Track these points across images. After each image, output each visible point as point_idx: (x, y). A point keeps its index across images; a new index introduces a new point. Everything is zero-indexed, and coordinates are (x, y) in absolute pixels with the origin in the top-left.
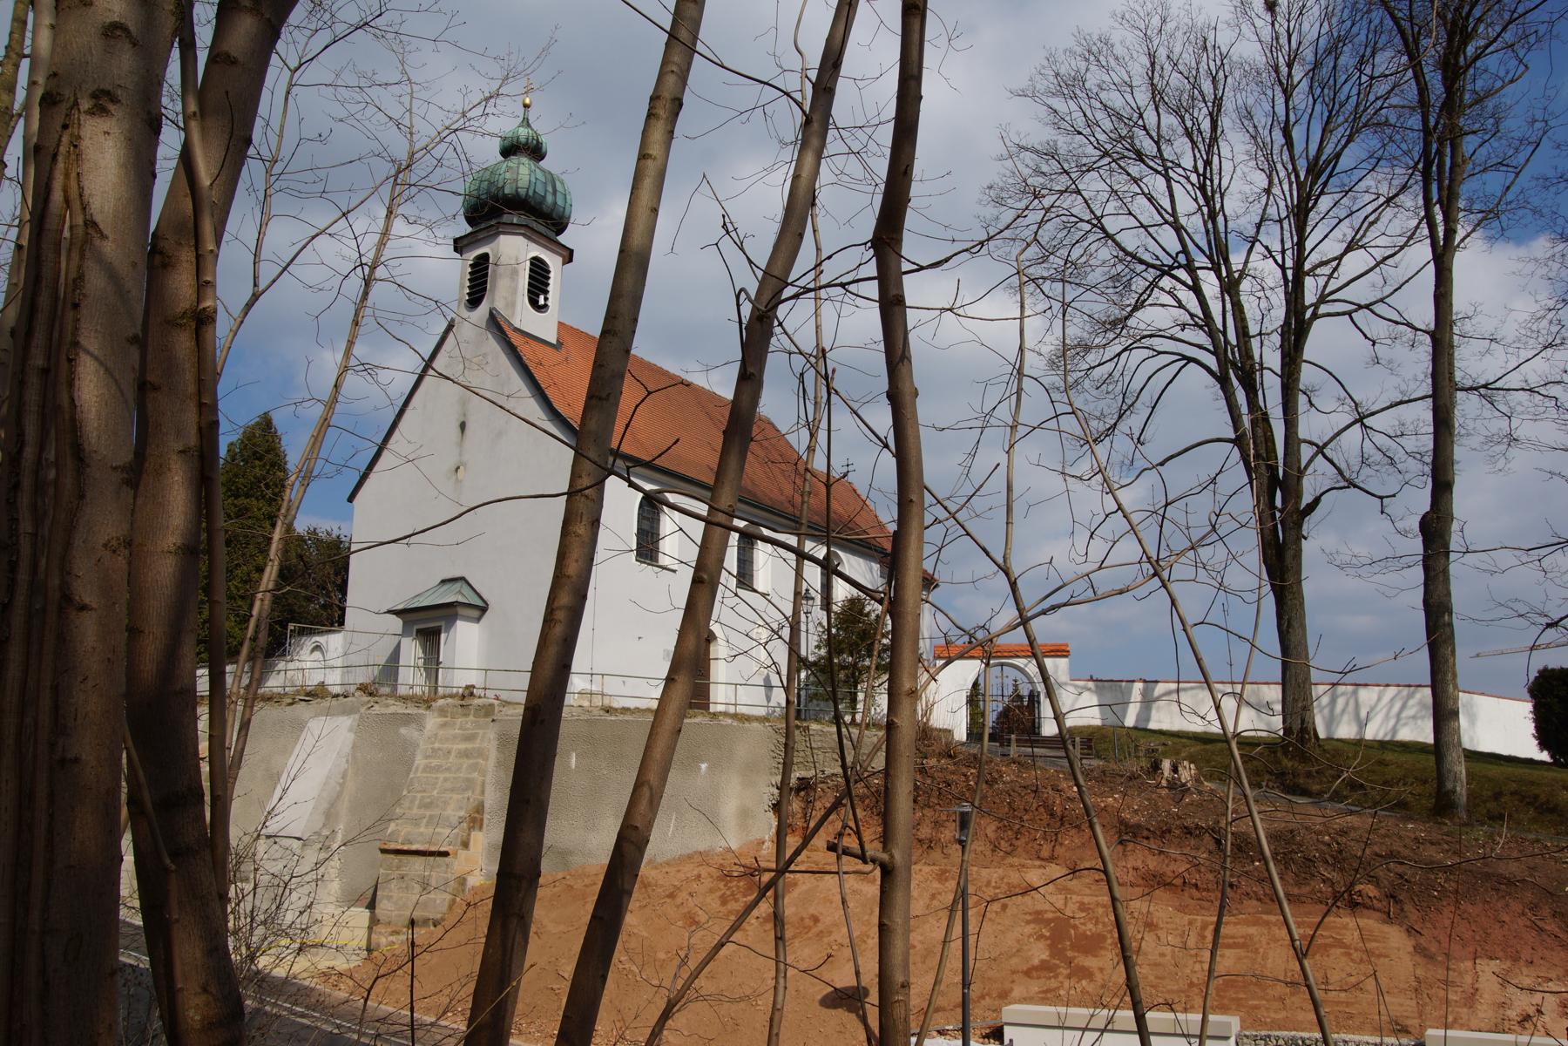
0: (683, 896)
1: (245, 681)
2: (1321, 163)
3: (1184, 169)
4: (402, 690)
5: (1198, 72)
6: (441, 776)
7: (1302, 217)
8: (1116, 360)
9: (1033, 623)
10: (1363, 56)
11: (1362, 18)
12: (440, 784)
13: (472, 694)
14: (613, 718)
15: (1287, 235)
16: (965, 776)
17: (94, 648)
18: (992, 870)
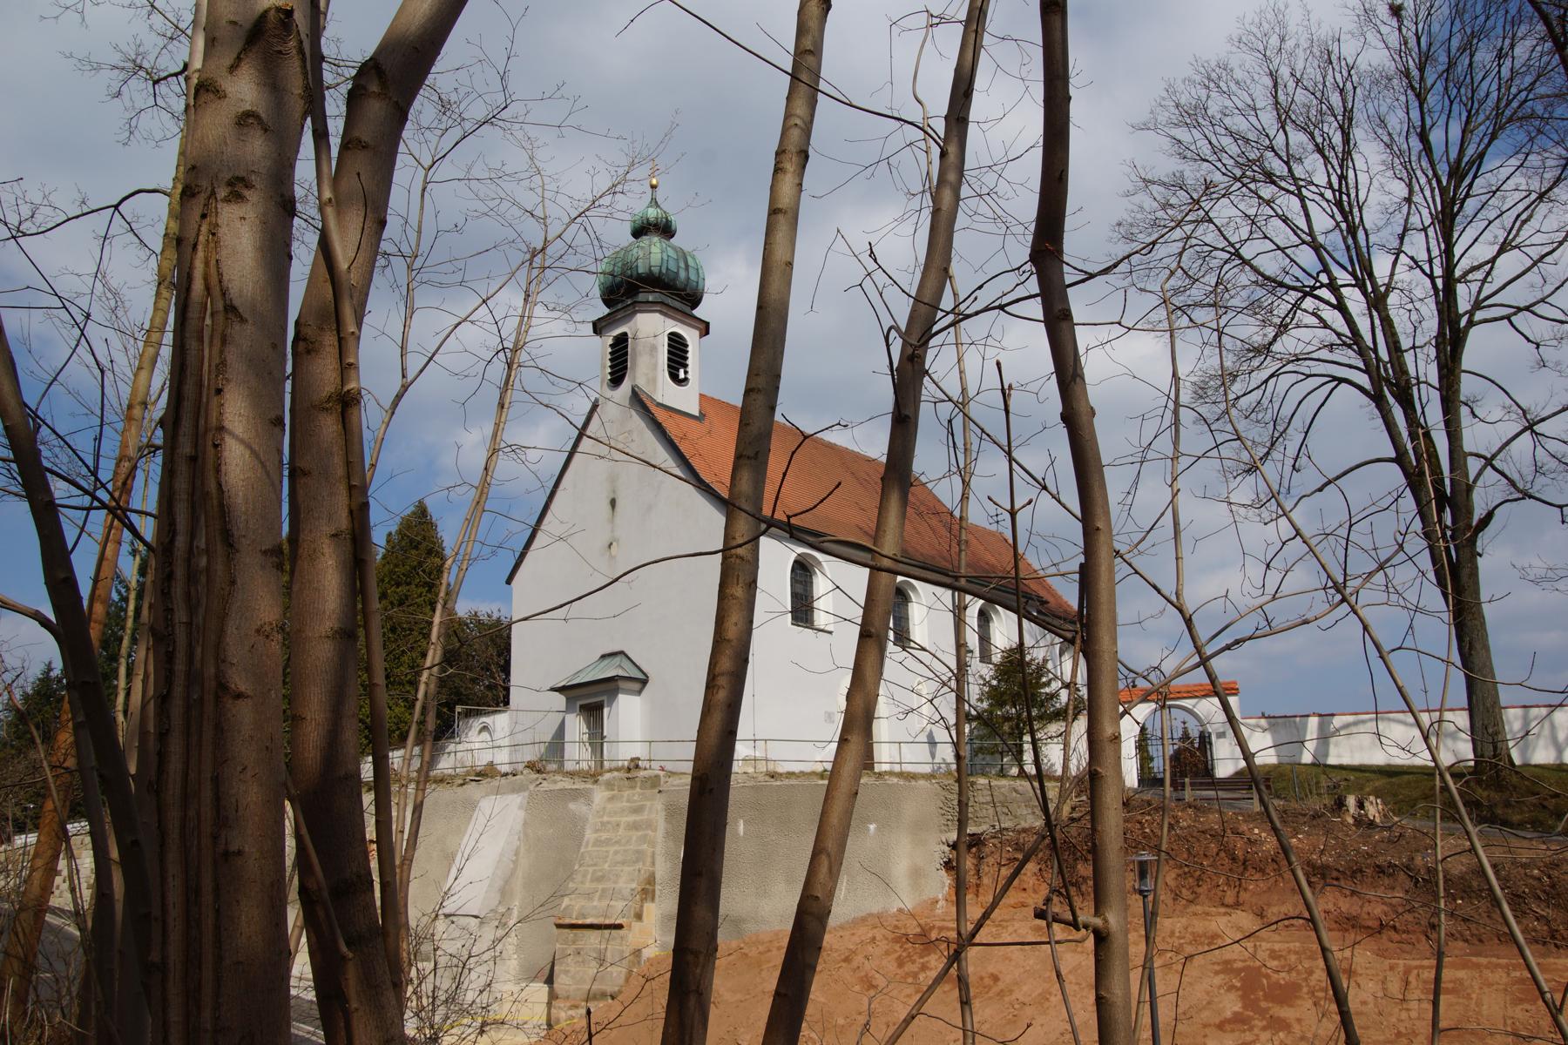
0: (858, 959)
1: (416, 764)
2: (1463, 165)
3: (1317, 186)
4: (569, 766)
5: (1324, 85)
6: (612, 849)
7: (1448, 223)
8: (1263, 387)
9: (1214, 663)
10: (1501, 49)
11: (1497, 11)
12: (610, 857)
13: (637, 767)
14: (778, 783)
15: (1433, 243)
16: (1140, 823)
17: (251, 737)
18: (1176, 919)
